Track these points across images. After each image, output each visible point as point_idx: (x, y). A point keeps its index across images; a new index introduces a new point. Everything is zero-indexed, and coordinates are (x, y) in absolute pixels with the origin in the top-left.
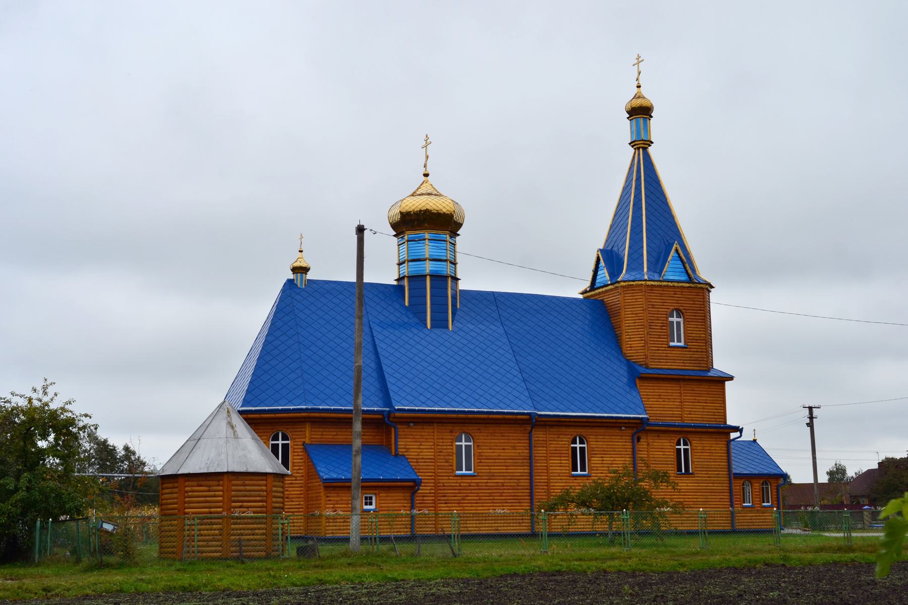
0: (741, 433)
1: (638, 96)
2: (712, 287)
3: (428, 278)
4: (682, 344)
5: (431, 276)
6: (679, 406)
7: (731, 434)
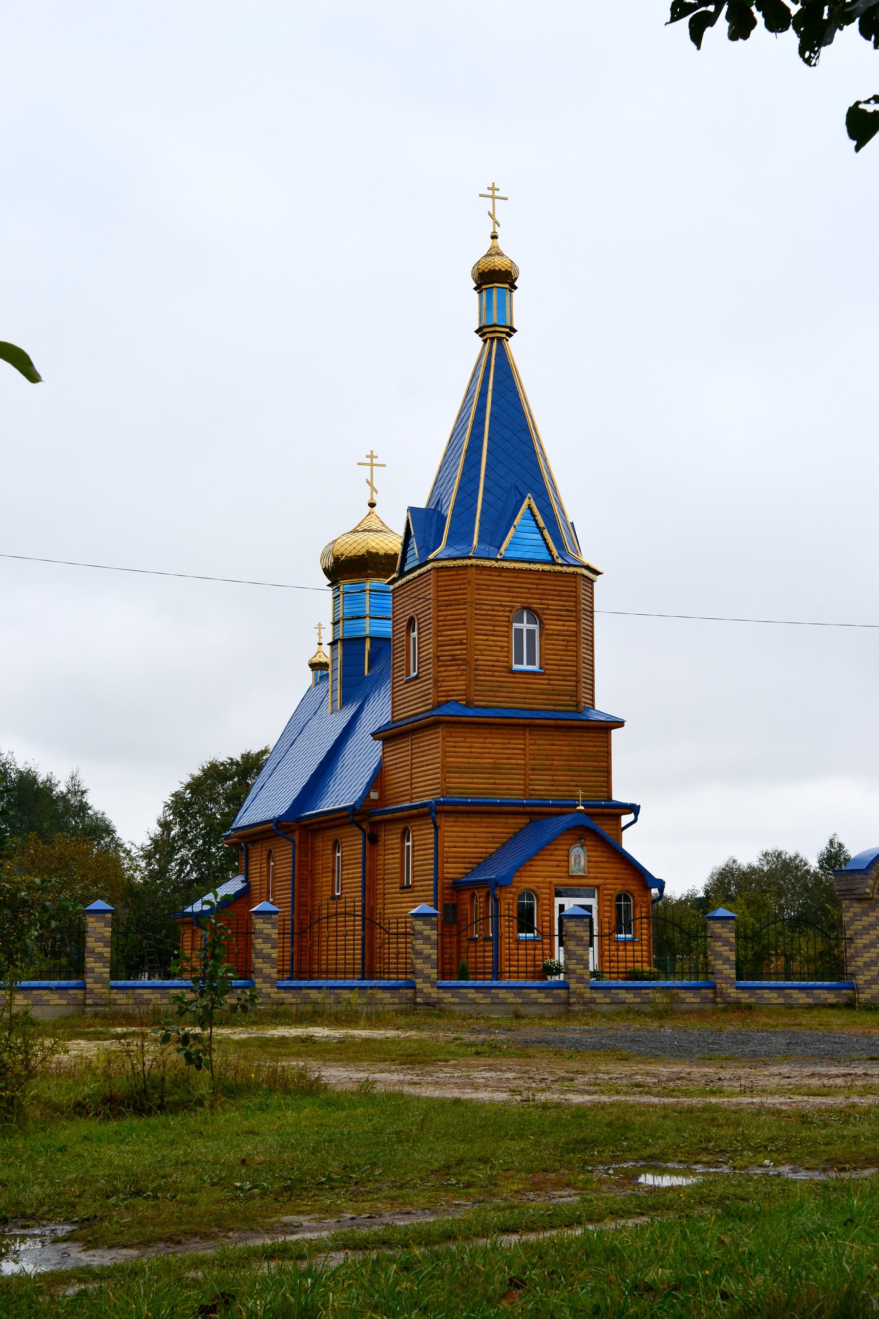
0: (636, 815)
1: (494, 252)
2: (597, 573)
4: (535, 668)
5: (372, 639)
6: (603, 784)
7: (623, 817)
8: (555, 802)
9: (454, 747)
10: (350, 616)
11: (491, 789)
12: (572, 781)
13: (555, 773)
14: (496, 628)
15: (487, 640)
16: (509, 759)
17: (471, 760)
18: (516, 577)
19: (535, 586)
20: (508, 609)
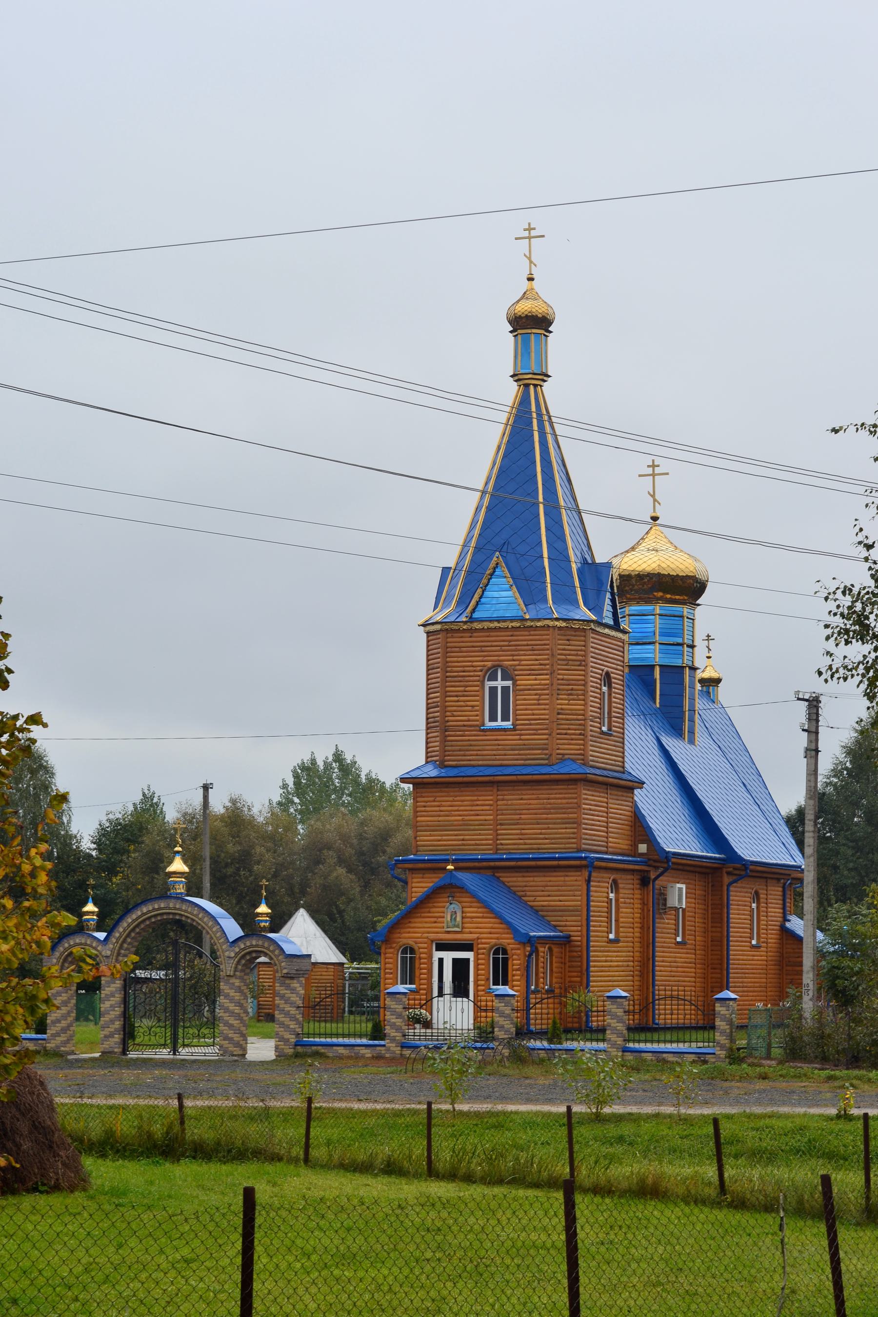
3: (657, 669)
4: (508, 724)
8: (509, 857)
9: (425, 807)
10: (634, 641)
11: (459, 845)
12: (541, 834)
13: (523, 826)
14: (467, 689)
15: (458, 701)
16: (478, 815)
17: (440, 818)
18: (488, 636)
19: (506, 643)
20: (479, 668)
